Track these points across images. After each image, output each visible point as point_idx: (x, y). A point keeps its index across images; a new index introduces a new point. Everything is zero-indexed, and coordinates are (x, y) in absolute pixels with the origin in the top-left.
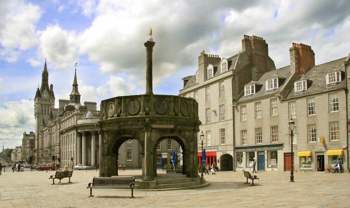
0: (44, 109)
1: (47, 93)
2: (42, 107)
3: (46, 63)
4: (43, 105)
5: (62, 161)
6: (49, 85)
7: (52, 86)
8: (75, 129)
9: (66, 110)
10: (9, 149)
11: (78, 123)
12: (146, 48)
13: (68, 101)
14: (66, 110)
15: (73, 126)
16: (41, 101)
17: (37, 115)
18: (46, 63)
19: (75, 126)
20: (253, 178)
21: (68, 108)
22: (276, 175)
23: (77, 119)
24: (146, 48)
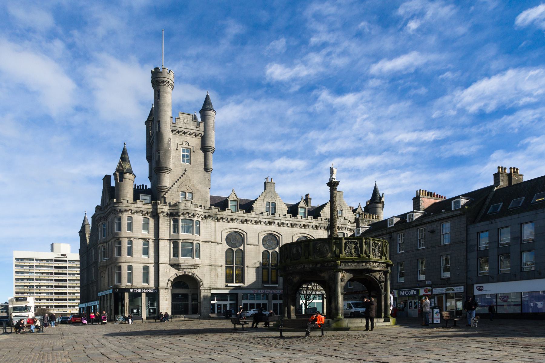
3: (376, 184)
18: (376, 184)
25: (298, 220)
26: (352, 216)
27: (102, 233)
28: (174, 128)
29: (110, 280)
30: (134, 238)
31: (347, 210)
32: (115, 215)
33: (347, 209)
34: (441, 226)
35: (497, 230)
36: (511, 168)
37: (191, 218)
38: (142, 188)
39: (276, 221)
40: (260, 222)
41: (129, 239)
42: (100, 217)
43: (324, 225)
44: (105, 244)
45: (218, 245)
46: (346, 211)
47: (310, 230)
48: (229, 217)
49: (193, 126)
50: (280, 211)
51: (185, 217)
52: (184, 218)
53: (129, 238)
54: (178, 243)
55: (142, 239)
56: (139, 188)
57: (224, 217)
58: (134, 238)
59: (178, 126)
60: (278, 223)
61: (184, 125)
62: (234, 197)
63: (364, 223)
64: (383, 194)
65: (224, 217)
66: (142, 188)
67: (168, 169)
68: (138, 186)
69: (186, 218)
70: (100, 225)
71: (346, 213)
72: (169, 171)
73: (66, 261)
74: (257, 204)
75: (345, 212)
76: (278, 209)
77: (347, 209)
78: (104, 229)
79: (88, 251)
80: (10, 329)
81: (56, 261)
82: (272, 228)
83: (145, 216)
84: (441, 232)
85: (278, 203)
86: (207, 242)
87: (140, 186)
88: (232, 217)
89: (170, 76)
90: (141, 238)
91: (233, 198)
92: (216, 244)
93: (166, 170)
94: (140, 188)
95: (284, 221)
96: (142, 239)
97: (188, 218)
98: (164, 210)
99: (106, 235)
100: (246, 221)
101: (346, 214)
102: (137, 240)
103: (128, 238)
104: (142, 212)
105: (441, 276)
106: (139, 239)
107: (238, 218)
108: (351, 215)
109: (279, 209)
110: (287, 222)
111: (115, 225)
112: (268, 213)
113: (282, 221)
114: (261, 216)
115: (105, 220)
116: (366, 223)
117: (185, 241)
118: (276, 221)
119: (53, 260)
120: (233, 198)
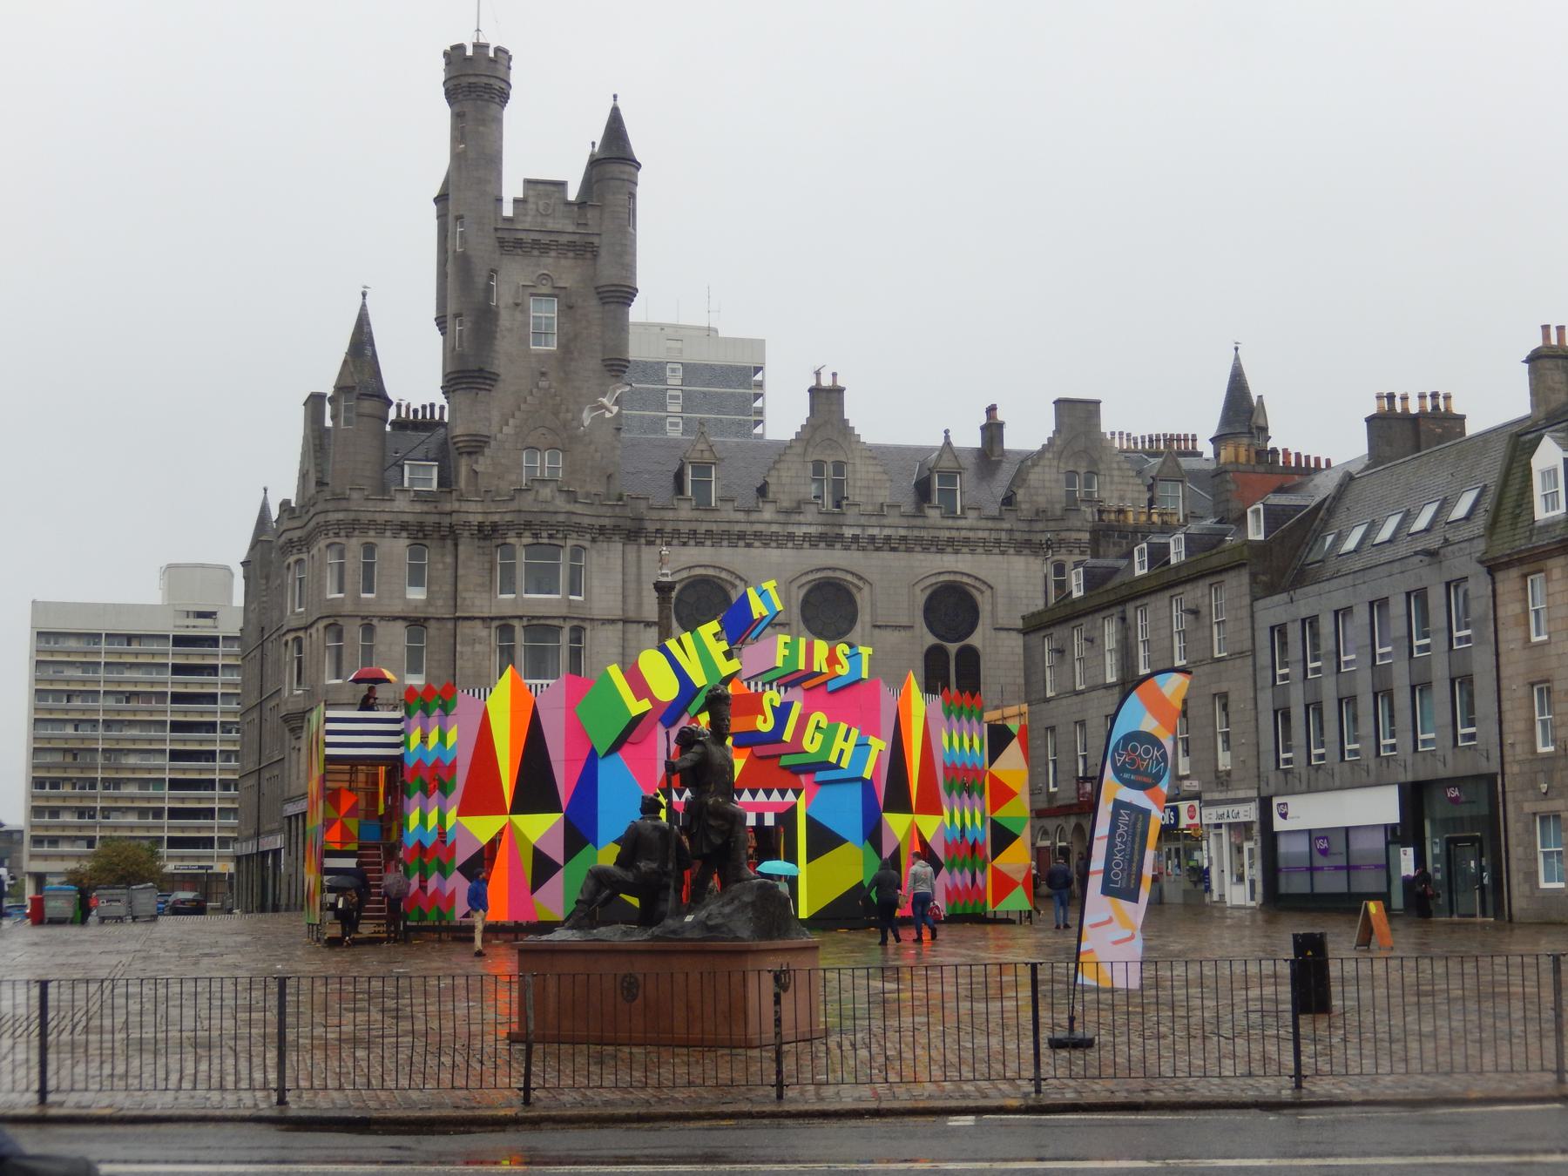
3: (1237, 358)
18: (1237, 358)
25: (930, 522)
26: (1136, 495)
27: (293, 600)
28: (506, 235)
29: (632, 586)
30: (382, 618)
31: (1116, 473)
32: (329, 541)
33: (1115, 466)
34: (1171, 605)
35: (1367, 608)
36: (1422, 397)
37: (557, 538)
38: (428, 417)
39: (848, 532)
40: (791, 537)
41: (366, 621)
42: (291, 541)
43: (1026, 536)
44: (301, 634)
45: (648, 629)
46: (1111, 476)
47: (976, 557)
48: (684, 528)
49: (567, 222)
50: (864, 492)
51: (535, 536)
52: (535, 541)
53: (367, 617)
54: (512, 628)
55: (404, 619)
56: (420, 417)
57: (669, 528)
58: (382, 618)
59: (519, 227)
60: (855, 538)
61: (539, 219)
62: (702, 451)
63: (1114, 544)
64: (1260, 397)
65: (669, 528)
66: (428, 417)
67: (487, 375)
68: (415, 411)
69: (541, 541)
70: (289, 565)
71: (1112, 483)
72: (488, 382)
73: (213, 641)
74: (783, 474)
75: (1108, 479)
76: (854, 487)
77: (1115, 466)
78: (301, 580)
79: (262, 644)
80: (618, 614)
81: (179, 641)
82: (836, 558)
83: (417, 538)
84: (1172, 626)
85: (858, 461)
86: (608, 620)
87: (424, 407)
88: (693, 526)
89: (498, 66)
90: (402, 615)
91: (699, 455)
92: (642, 625)
93: (479, 380)
94: (424, 416)
95: (875, 531)
96: (404, 619)
97: (546, 541)
98: (471, 518)
99: (304, 601)
100: (742, 536)
101: (1114, 487)
102: (391, 623)
103: (363, 618)
104: (404, 527)
105: (1217, 766)
106: (395, 618)
107: (714, 527)
108: (1135, 488)
109: (859, 484)
110: (887, 532)
111: (328, 575)
112: (820, 502)
113: (871, 531)
114: (796, 518)
115: (304, 549)
116: (1124, 541)
117: (535, 622)
118: (848, 532)
119: (167, 637)
120: (699, 455)
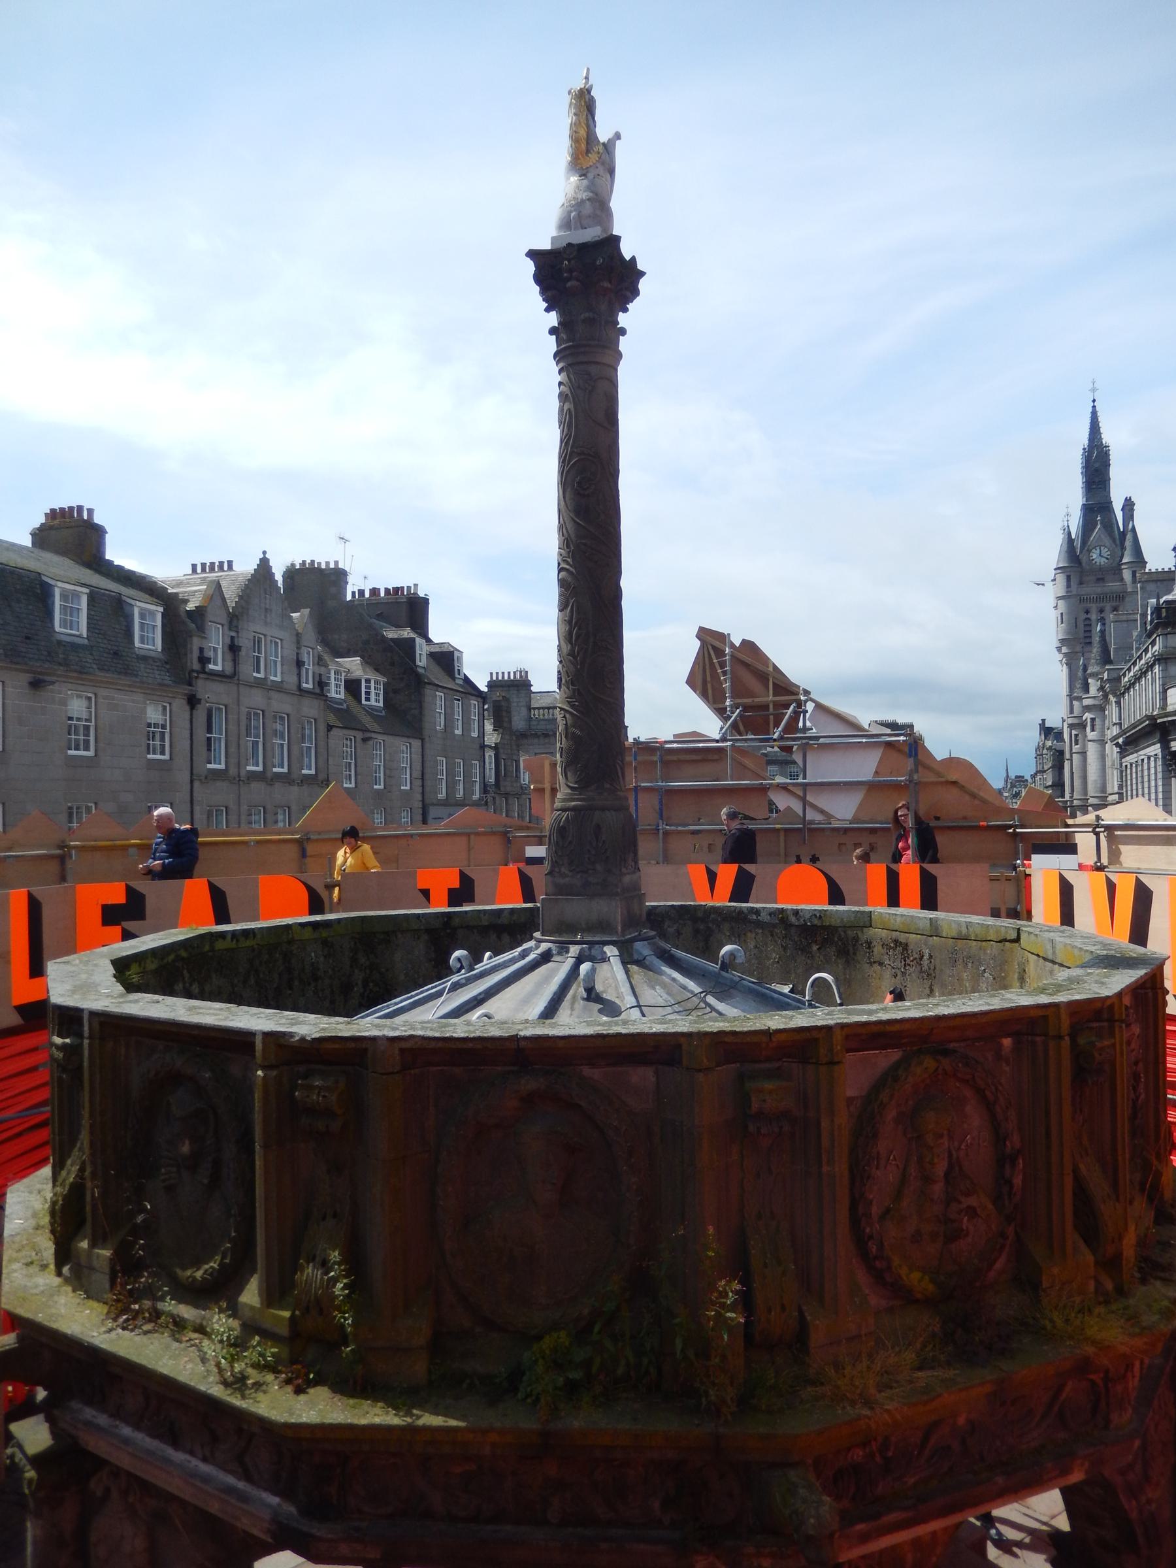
0: (1094, 616)
1: (1107, 541)
2: (1087, 612)
3: (1094, 407)
4: (1090, 600)
5: (420, 654)
6: (1117, 505)
7: (1129, 505)
8: (1158, 735)
9: (1156, 627)
10: (337, 576)
11: (1169, 701)
12: (553, 319)
13: (1161, 577)
14: (1156, 627)
15: (1140, 722)
16: (1081, 583)
17: (1064, 650)
18: (1094, 407)
19: (1152, 718)
20: (316, 703)
21: (1164, 614)
22: (590, 872)
23: (1163, 685)
24: (553, 319)
